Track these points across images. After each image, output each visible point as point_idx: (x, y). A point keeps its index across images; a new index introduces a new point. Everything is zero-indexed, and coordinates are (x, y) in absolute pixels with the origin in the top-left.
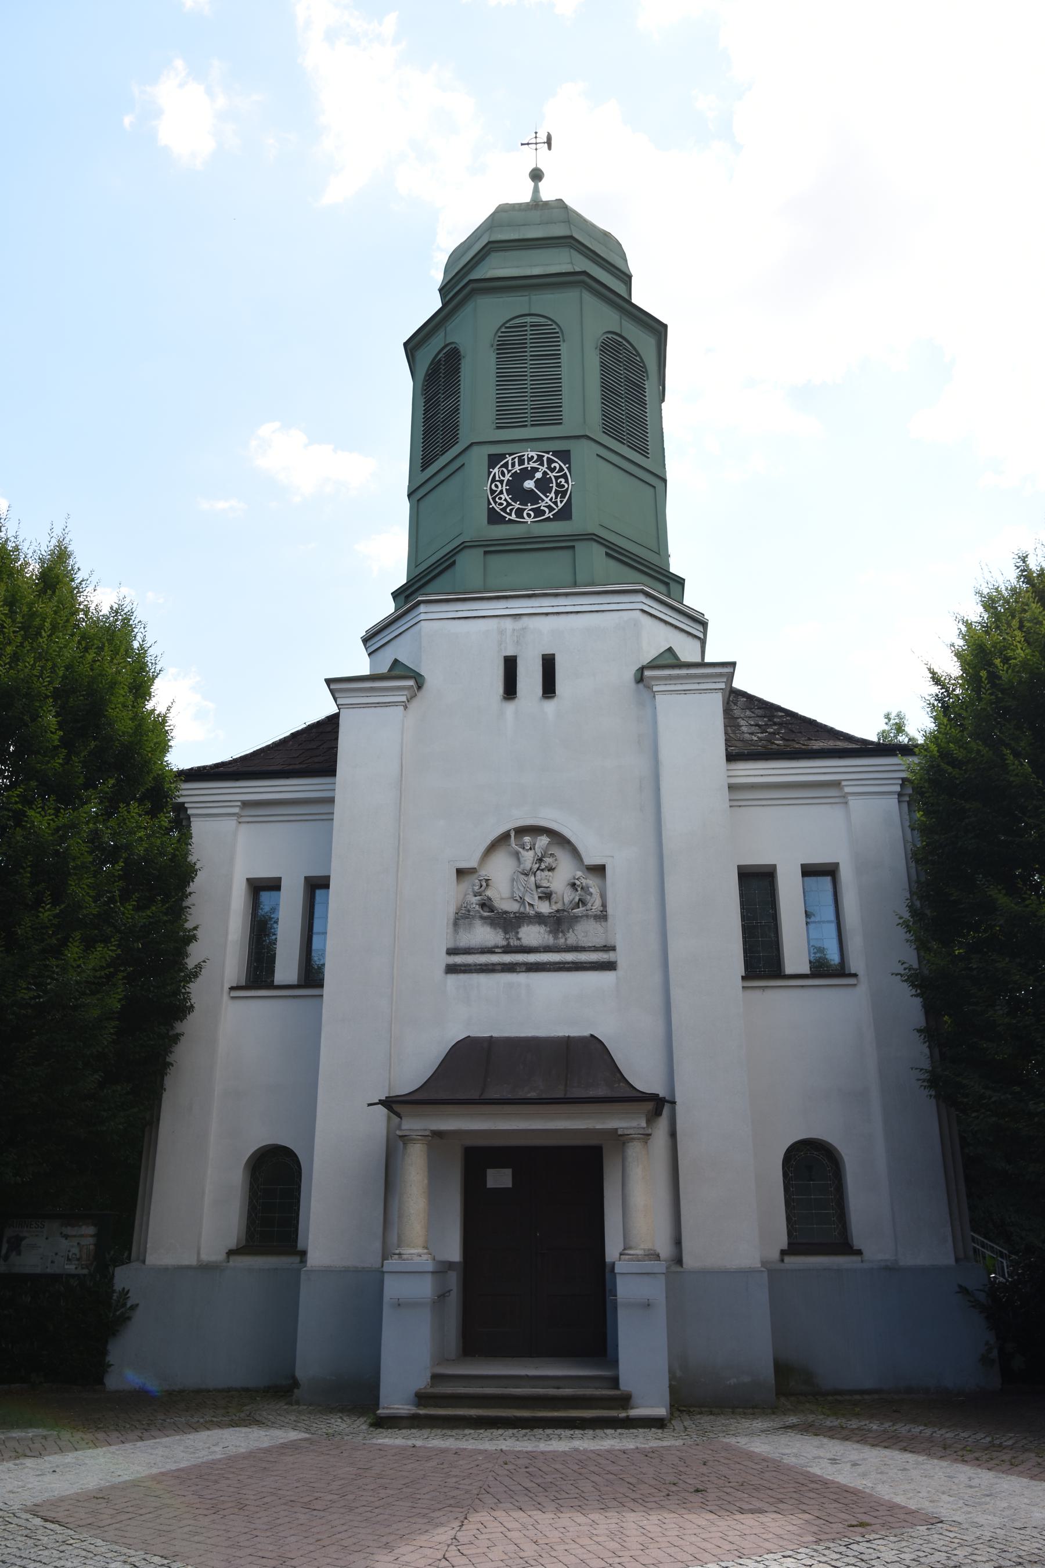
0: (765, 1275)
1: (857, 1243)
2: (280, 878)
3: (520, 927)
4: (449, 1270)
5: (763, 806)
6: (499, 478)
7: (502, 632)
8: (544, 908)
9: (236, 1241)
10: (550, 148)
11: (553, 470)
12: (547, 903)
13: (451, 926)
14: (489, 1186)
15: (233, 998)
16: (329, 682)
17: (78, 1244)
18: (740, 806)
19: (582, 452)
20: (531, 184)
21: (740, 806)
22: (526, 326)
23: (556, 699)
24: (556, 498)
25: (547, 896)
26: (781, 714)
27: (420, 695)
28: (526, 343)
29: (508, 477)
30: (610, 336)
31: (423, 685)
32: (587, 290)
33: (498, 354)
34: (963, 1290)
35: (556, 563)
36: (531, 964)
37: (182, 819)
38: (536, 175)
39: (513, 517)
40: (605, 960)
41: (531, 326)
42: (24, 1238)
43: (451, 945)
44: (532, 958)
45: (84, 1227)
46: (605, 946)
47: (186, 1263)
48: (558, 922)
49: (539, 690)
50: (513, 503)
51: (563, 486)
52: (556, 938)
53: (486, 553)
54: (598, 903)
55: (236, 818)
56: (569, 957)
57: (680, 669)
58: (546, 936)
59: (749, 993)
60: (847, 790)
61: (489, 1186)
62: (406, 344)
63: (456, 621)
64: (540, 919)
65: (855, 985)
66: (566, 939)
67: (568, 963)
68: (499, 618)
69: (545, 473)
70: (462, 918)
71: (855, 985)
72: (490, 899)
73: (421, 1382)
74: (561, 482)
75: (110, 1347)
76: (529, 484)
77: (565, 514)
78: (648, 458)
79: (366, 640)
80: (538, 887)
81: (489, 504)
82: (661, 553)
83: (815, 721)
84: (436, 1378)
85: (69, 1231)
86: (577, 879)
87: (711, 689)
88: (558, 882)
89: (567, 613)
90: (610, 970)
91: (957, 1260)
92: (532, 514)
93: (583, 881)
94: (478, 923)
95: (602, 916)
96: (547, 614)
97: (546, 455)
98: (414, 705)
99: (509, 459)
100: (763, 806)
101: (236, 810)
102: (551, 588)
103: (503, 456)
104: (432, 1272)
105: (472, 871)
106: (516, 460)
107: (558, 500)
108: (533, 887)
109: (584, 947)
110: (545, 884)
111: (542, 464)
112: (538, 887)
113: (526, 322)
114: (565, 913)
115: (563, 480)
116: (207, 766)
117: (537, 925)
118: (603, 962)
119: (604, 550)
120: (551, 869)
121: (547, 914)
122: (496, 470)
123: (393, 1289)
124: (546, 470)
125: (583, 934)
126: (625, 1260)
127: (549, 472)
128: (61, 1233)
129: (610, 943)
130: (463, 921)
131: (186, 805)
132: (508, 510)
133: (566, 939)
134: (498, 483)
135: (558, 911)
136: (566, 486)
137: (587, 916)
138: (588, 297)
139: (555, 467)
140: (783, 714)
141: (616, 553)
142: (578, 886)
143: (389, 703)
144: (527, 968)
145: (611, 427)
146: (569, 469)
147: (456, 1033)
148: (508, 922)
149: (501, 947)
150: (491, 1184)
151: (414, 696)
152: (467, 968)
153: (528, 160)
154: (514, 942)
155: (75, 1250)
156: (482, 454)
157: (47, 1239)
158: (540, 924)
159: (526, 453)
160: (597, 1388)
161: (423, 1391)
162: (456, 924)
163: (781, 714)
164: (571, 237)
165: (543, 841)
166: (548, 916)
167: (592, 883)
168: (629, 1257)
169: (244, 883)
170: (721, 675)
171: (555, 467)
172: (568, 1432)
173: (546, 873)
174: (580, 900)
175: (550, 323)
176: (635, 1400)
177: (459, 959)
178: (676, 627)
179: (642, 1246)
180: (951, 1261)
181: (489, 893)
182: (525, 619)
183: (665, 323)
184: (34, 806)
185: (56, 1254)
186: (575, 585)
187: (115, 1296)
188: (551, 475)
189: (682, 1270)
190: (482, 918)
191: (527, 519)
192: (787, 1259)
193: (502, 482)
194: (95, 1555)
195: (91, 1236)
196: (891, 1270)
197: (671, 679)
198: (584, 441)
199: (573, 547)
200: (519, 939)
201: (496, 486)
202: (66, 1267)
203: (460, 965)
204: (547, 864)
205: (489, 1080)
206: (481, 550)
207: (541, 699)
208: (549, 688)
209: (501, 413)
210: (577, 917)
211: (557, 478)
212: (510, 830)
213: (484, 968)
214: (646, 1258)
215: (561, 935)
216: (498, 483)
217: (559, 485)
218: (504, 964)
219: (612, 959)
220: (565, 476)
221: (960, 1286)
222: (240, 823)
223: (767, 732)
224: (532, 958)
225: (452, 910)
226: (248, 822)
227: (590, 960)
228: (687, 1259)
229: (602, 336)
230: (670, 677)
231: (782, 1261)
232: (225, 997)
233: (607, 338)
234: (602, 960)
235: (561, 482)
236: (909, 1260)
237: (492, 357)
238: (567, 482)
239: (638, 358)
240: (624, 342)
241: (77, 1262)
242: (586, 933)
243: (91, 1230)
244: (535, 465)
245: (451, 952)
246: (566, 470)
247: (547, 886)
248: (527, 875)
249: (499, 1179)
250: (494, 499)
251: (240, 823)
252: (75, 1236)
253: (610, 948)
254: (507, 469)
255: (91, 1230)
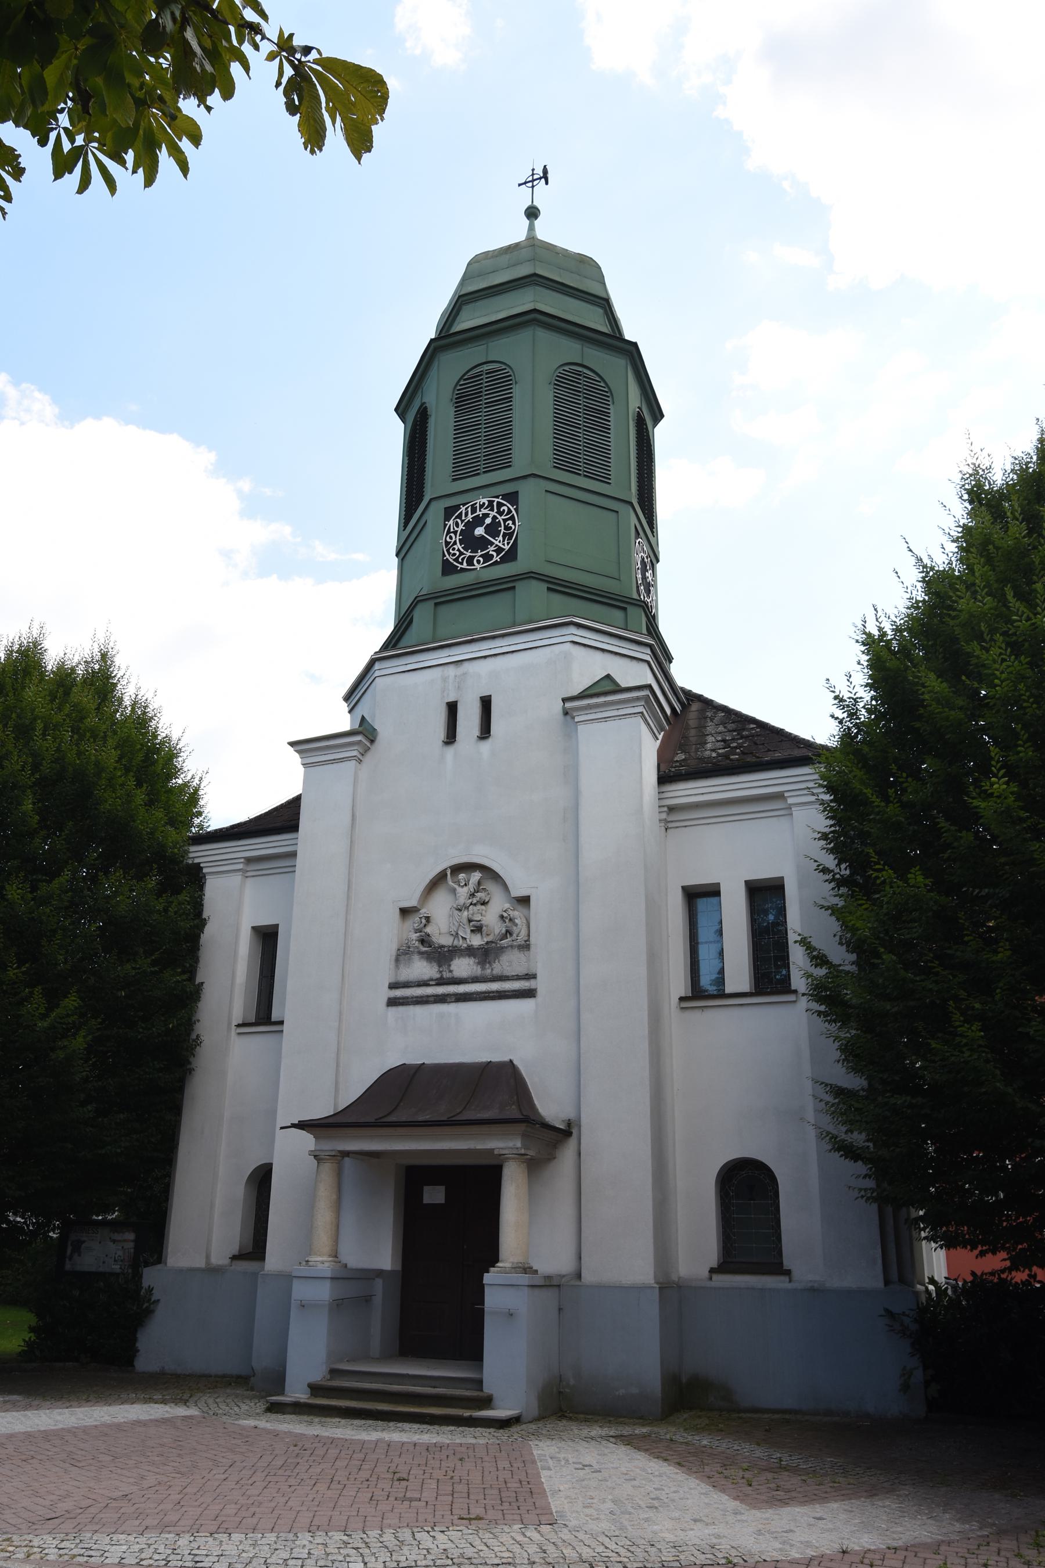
0: (657, 1291)
1: (787, 1264)
2: (277, 926)
3: (452, 960)
4: (377, 1277)
5: (708, 824)
6: (454, 529)
7: (445, 679)
8: (476, 941)
9: (238, 1248)
10: (547, 183)
11: (501, 513)
12: (479, 936)
13: (393, 962)
14: (425, 1202)
15: (682, 1008)
16: (292, 744)
17: (123, 1247)
18: (686, 826)
19: (528, 491)
20: (526, 222)
21: (686, 826)
22: (481, 375)
23: (490, 740)
24: (504, 541)
25: (478, 929)
26: (752, 726)
27: (373, 748)
28: (481, 392)
29: (461, 527)
30: (566, 368)
31: (375, 738)
32: (539, 326)
33: (456, 407)
34: (889, 1313)
35: (496, 607)
36: (461, 994)
37: (196, 877)
38: (532, 213)
39: (465, 566)
40: (526, 988)
41: (487, 374)
42: (84, 1242)
43: (393, 980)
44: (461, 989)
45: (127, 1233)
46: (527, 975)
47: (198, 1266)
48: (486, 954)
49: (476, 731)
50: (465, 552)
51: (511, 528)
52: (483, 969)
53: (436, 604)
54: (524, 932)
55: (241, 873)
56: (495, 986)
57: (598, 697)
58: (475, 967)
59: (688, 1014)
60: (790, 801)
61: (425, 1202)
62: (396, 410)
63: (406, 673)
64: (470, 951)
65: (795, 1002)
66: (492, 970)
67: (493, 992)
68: (443, 666)
69: (495, 518)
70: (403, 955)
71: (795, 1002)
72: (429, 935)
73: (318, 1374)
74: (508, 524)
75: (139, 1335)
76: (479, 531)
77: (511, 556)
78: (609, 483)
79: (347, 698)
80: (470, 921)
81: (444, 555)
82: (621, 579)
83: (782, 730)
84: (334, 1372)
85: (116, 1236)
86: (505, 911)
87: (630, 714)
88: (490, 917)
89: (503, 653)
90: (530, 997)
91: (887, 1282)
92: (481, 560)
93: (511, 913)
94: (416, 957)
95: (526, 946)
96: (485, 657)
97: (496, 500)
98: (368, 759)
99: (463, 509)
100: (708, 824)
101: (241, 866)
102: (488, 631)
103: (458, 507)
104: (331, 1278)
105: (415, 909)
106: (469, 509)
107: (506, 542)
108: (465, 921)
109: (508, 977)
110: (477, 917)
111: (492, 510)
112: (470, 921)
113: (482, 371)
114: (493, 945)
115: (510, 522)
116: (224, 828)
117: (467, 957)
118: (525, 990)
119: (545, 586)
120: (484, 903)
121: (476, 947)
122: (451, 522)
123: (300, 1291)
124: (496, 514)
125: (507, 964)
126: (494, 1272)
127: (498, 516)
128: (110, 1238)
129: (532, 971)
130: (403, 956)
131: (202, 865)
132: (460, 560)
133: (492, 970)
134: (452, 535)
135: (487, 943)
136: (513, 527)
137: (512, 946)
138: (542, 334)
139: (504, 510)
140: (755, 726)
141: (558, 586)
142: (506, 918)
143: (343, 758)
144: (456, 999)
145: (564, 460)
146: (516, 510)
147: (394, 1061)
148: (441, 955)
149: (435, 980)
150: (427, 1200)
151: (367, 750)
152: (405, 1001)
153: (523, 199)
154: (446, 975)
155: (120, 1253)
156: (438, 508)
157: (100, 1243)
158: (469, 956)
159: (478, 501)
160: (467, 1390)
161: (320, 1383)
162: (397, 960)
163: (752, 726)
164: (535, 275)
165: (476, 876)
166: (478, 948)
167: (517, 914)
168: (499, 1269)
169: (680, 891)
170: (638, 699)
171: (504, 510)
172: (416, 1426)
173: (479, 907)
174: (507, 931)
175: (504, 367)
176: (496, 1402)
177: (399, 993)
178: (616, 654)
179: (511, 1260)
180: (880, 1284)
181: (428, 930)
182: (466, 665)
183: (634, 341)
184: (10, 882)
185: (107, 1256)
186: (514, 625)
187: (143, 1292)
188: (500, 518)
189: (580, 1284)
190: (420, 953)
191: (477, 566)
192: (715, 1277)
193: (455, 533)
194: (740, 1556)
195: (132, 1241)
196: (815, 1291)
197: (591, 709)
198: (532, 480)
199: (514, 588)
200: (451, 971)
201: (451, 538)
202: (113, 1267)
203: (399, 998)
204: (478, 899)
205: (402, 1104)
206: (431, 603)
207: (477, 740)
208: (485, 731)
209: (457, 465)
210: (503, 948)
211: (505, 521)
212: (446, 869)
213: (419, 999)
214: (513, 1270)
215: (488, 965)
216: (452, 535)
217: (507, 528)
218: (437, 996)
219: (533, 987)
220: (512, 518)
221: (887, 1310)
222: (247, 877)
223: (730, 747)
224: (461, 989)
225: (394, 947)
226: (253, 876)
227: (513, 989)
228: (585, 1274)
229: (554, 372)
230: (589, 707)
231: (711, 1279)
232: (233, 1033)
233: (564, 370)
234: (524, 988)
235: (508, 524)
236: (836, 1282)
237: (452, 410)
238: (514, 523)
239: (602, 384)
240: (585, 371)
241: (121, 1263)
242: (511, 962)
243: (131, 1236)
244: (486, 511)
245: (393, 986)
246: (514, 512)
247: (478, 919)
248: (460, 910)
249: (434, 1195)
250: (448, 551)
251: (247, 877)
252: (119, 1241)
253: (531, 976)
254: (461, 519)
255: (131, 1236)
